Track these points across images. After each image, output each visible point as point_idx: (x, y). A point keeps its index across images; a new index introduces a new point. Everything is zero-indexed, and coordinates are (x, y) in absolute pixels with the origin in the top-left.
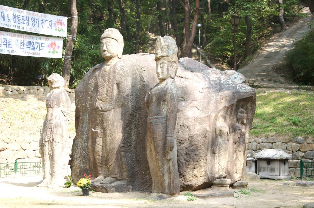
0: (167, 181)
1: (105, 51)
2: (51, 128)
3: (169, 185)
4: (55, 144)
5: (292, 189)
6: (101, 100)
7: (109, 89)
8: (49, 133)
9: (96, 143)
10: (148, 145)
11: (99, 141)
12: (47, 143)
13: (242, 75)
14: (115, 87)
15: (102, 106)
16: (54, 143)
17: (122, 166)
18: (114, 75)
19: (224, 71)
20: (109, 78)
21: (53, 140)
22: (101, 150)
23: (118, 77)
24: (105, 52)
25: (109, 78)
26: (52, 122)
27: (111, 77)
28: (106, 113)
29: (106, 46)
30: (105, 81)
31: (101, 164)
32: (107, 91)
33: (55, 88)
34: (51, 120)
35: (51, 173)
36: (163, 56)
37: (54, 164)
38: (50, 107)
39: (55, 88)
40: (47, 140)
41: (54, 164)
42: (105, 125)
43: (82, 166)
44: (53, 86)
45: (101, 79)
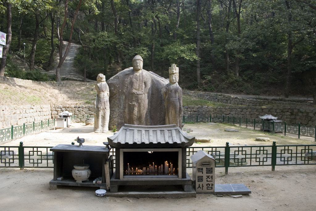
0: (255, 100)
1: (138, 66)
2: (104, 102)
3: (256, 99)
4: (106, 110)
5: (231, 129)
6: (136, 89)
7: (140, 84)
8: (103, 105)
9: (134, 110)
10: (170, 111)
11: (136, 109)
12: (101, 110)
13: (74, 44)
14: (143, 84)
15: (137, 92)
16: (106, 110)
17: (147, 120)
18: (143, 78)
19: (285, 102)
20: (140, 79)
21: (105, 108)
22: (136, 113)
23: (145, 80)
24: (138, 67)
25: (140, 79)
26: (104, 99)
27: (141, 79)
28: (140, 96)
29: (139, 64)
30: (137, 80)
31: (136, 120)
32: (139, 85)
33: (103, 81)
34: (104, 98)
35: (102, 125)
36: (176, 73)
37: (105, 121)
38: (102, 91)
39: (103, 81)
40: (102, 108)
41: (105, 121)
42: (140, 101)
43: (120, 121)
44: (102, 80)
45: (134, 79)
